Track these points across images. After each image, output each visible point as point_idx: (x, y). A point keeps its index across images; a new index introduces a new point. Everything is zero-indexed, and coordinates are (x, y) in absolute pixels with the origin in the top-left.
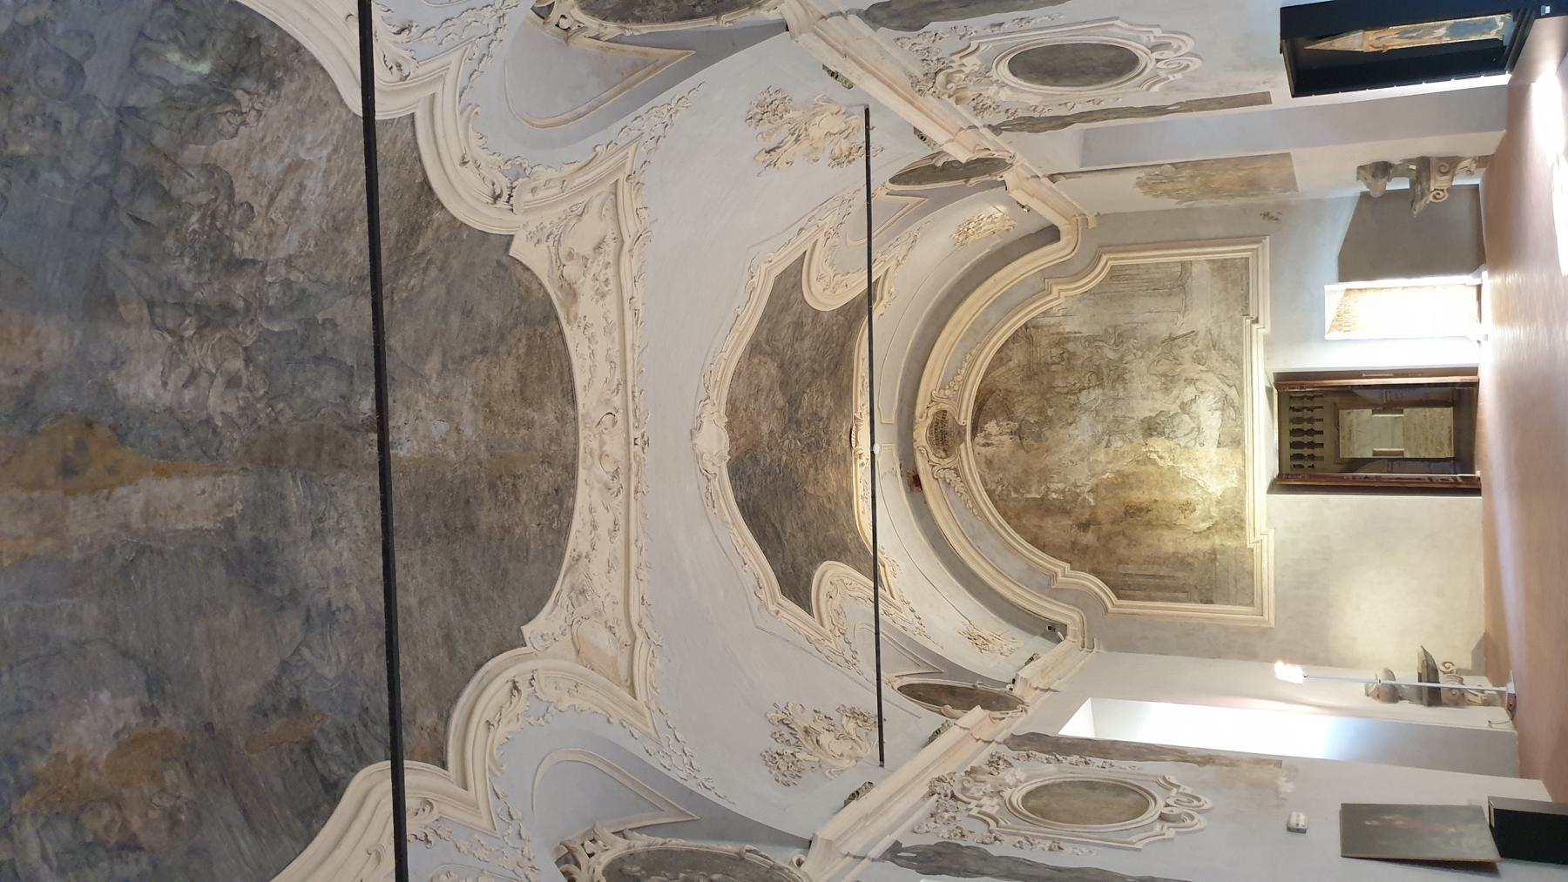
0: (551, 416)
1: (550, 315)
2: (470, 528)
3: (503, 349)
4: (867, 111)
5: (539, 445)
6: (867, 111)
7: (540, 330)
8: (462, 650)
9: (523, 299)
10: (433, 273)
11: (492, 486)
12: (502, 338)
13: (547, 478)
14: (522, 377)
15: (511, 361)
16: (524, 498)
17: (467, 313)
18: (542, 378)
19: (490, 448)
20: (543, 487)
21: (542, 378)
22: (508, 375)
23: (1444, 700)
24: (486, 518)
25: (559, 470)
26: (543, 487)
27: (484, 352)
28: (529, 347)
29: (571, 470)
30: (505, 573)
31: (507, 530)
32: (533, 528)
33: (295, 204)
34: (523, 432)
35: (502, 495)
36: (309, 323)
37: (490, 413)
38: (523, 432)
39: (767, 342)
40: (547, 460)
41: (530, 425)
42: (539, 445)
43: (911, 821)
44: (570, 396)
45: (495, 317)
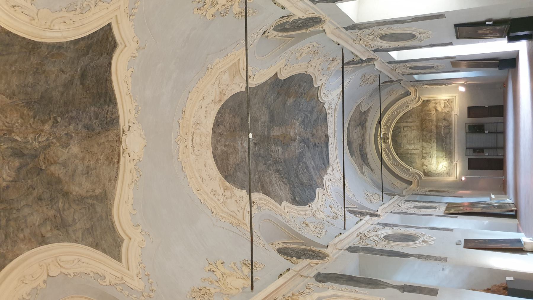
0: (219, 149)
1: (226, 178)
2: (242, 119)
3: (234, 166)
4: (252, 289)
5: (223, 140)
6: (252, 289)
7: (227, 174)
8: (255, 91)
9: (234, 181)
10: (254, 180)
11: (235, 129)
12: (235, 169)
13: (221, 129)
14: (228, 160)
15: (231, 163)
16: (228, 124)
17: (245, 173)
18: (223, 160)
19: (235, 139)
20: (222, 127)
21: (223, 160)
22: (232, 159)
23: (501, 104)
24: (238, 121)
25: (217, 131)
26: (222, 127)
27: (238, 165)
28: (228, 168)
29: (214, 132)
30: (238, 106)
31: (234, 116)
32: (227, 115)
33: (276, 183)
34: (227, 143)
35: (233, 126)
36: (266, 164)
37: (234, 148)
38: (227, 143)
39: (92, 205)
40: (221, 135)
41: (225, 146)
42: (223, 140)
43: (319, 10)
44: (214, 156)
45: (239, 174)
